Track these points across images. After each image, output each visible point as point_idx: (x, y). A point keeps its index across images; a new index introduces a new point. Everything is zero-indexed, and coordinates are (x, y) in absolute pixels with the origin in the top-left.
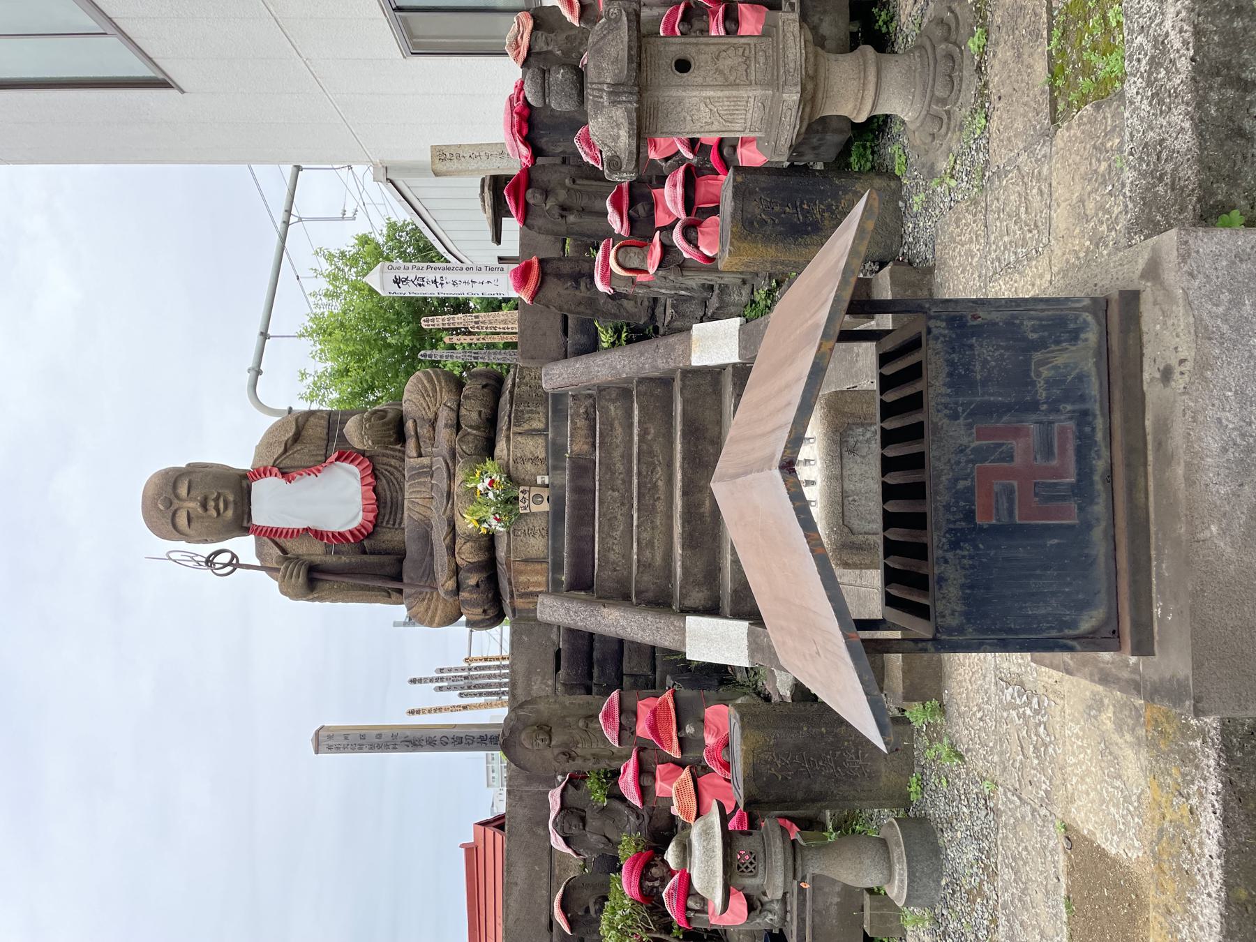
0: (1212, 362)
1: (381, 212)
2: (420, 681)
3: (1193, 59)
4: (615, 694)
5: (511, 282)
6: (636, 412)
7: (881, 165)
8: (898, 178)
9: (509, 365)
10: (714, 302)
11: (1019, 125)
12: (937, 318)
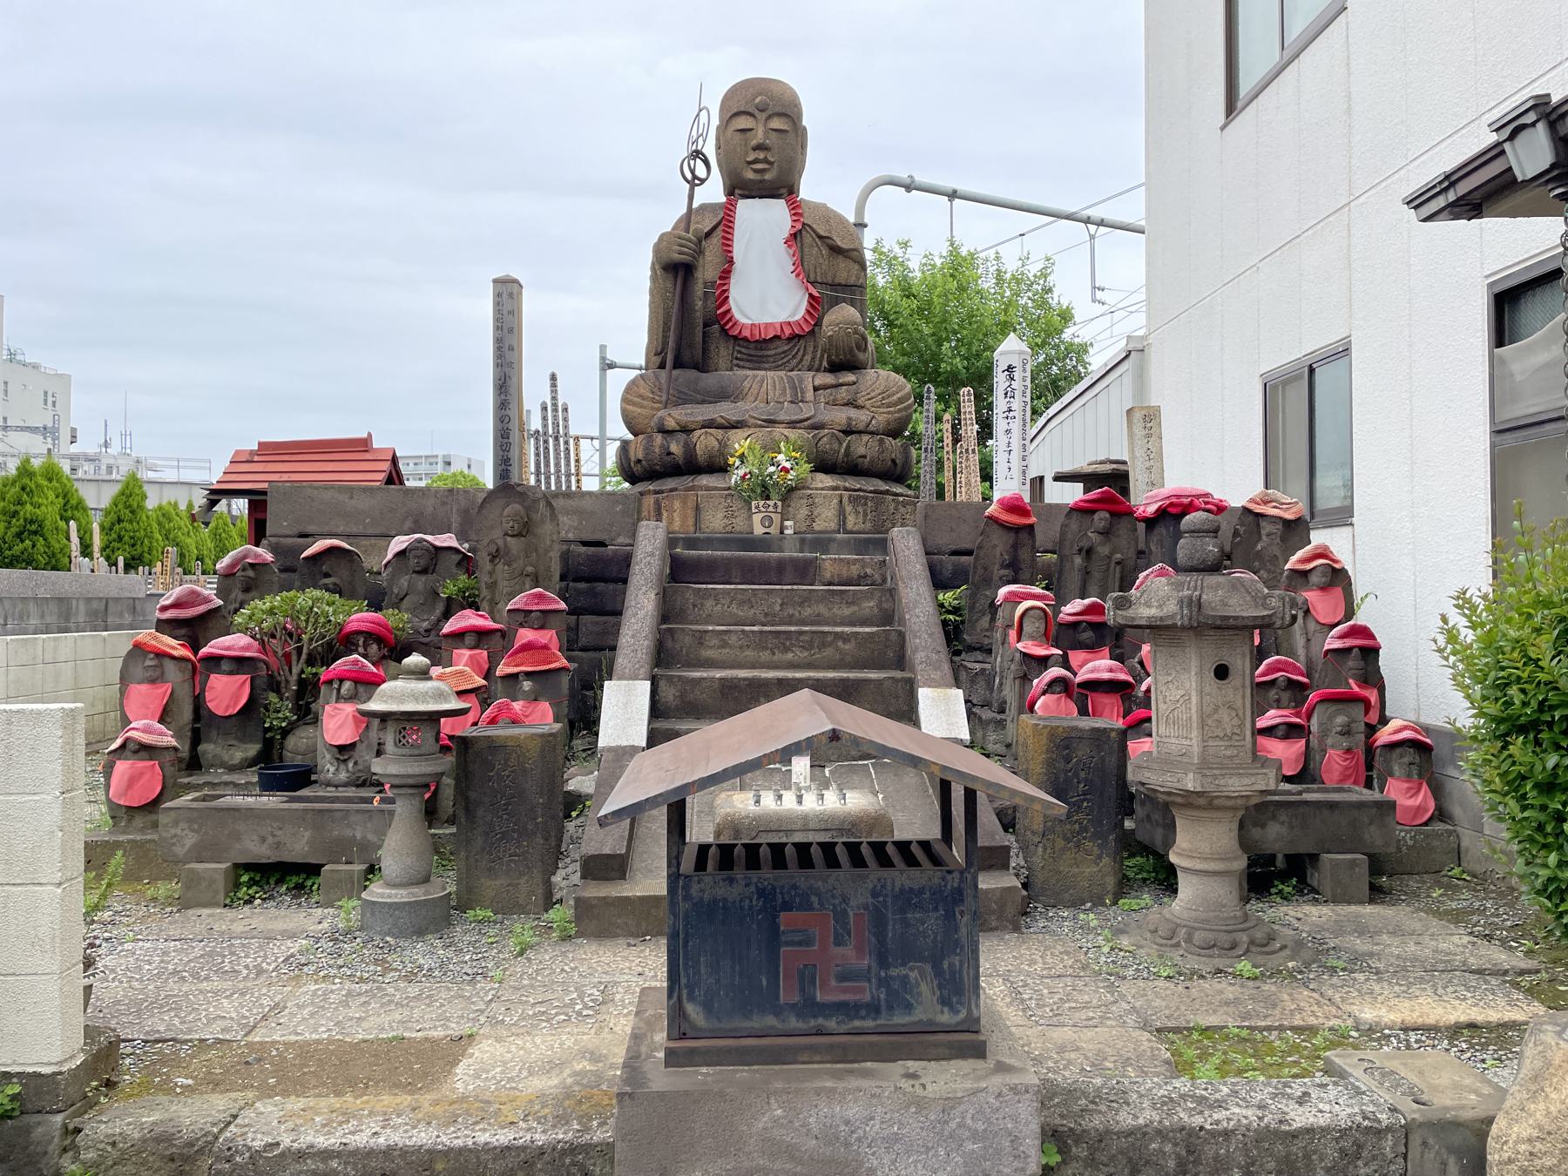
0: (924, 1112)
1: (1099, 337)
2: (554, 385)
3: (1202, 1128)
4: (563, 605)
5: (1008, 494)
6: (867, 630)
7: (1131, 888)
8: (1115, 903)
9: (917, 488)
10: (986, 714)
11: (1157, 1003)
12: (961, 880)
